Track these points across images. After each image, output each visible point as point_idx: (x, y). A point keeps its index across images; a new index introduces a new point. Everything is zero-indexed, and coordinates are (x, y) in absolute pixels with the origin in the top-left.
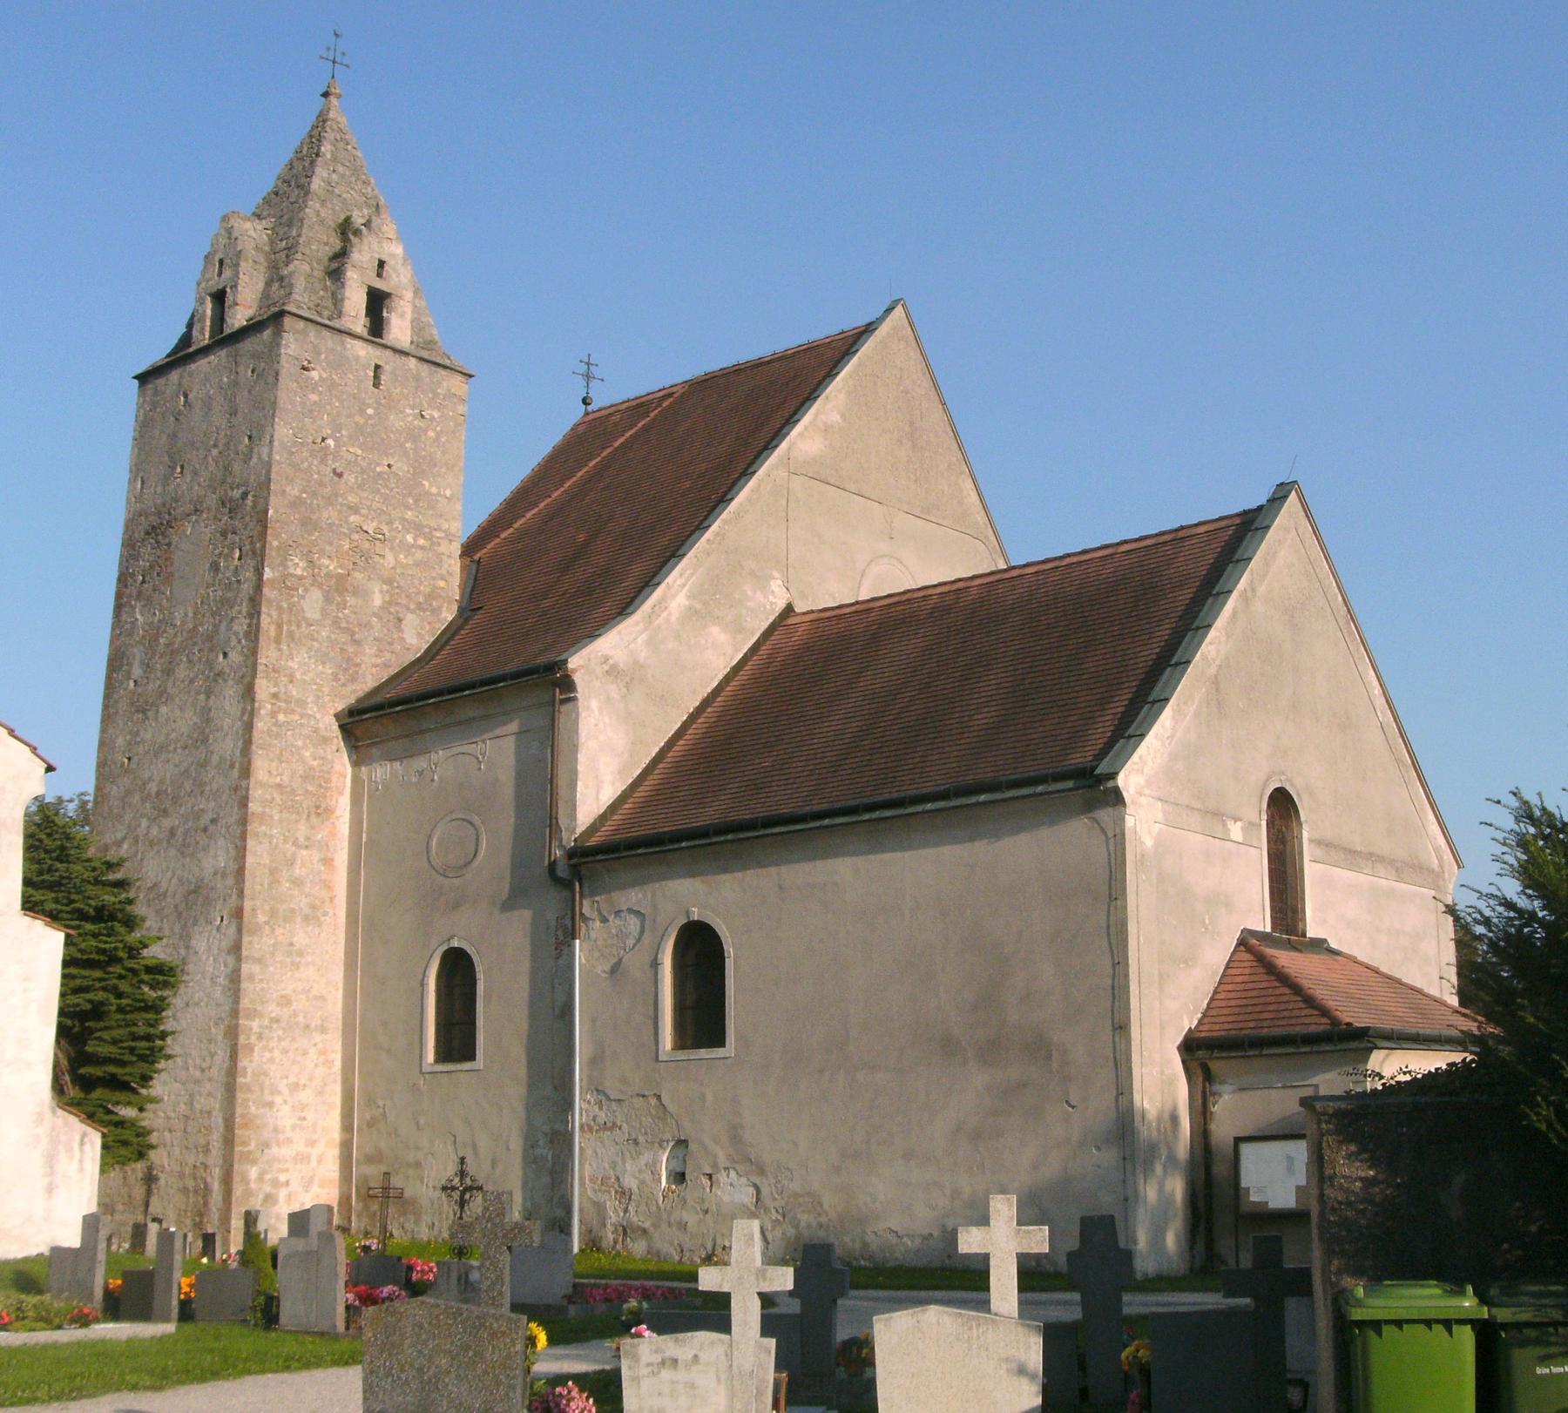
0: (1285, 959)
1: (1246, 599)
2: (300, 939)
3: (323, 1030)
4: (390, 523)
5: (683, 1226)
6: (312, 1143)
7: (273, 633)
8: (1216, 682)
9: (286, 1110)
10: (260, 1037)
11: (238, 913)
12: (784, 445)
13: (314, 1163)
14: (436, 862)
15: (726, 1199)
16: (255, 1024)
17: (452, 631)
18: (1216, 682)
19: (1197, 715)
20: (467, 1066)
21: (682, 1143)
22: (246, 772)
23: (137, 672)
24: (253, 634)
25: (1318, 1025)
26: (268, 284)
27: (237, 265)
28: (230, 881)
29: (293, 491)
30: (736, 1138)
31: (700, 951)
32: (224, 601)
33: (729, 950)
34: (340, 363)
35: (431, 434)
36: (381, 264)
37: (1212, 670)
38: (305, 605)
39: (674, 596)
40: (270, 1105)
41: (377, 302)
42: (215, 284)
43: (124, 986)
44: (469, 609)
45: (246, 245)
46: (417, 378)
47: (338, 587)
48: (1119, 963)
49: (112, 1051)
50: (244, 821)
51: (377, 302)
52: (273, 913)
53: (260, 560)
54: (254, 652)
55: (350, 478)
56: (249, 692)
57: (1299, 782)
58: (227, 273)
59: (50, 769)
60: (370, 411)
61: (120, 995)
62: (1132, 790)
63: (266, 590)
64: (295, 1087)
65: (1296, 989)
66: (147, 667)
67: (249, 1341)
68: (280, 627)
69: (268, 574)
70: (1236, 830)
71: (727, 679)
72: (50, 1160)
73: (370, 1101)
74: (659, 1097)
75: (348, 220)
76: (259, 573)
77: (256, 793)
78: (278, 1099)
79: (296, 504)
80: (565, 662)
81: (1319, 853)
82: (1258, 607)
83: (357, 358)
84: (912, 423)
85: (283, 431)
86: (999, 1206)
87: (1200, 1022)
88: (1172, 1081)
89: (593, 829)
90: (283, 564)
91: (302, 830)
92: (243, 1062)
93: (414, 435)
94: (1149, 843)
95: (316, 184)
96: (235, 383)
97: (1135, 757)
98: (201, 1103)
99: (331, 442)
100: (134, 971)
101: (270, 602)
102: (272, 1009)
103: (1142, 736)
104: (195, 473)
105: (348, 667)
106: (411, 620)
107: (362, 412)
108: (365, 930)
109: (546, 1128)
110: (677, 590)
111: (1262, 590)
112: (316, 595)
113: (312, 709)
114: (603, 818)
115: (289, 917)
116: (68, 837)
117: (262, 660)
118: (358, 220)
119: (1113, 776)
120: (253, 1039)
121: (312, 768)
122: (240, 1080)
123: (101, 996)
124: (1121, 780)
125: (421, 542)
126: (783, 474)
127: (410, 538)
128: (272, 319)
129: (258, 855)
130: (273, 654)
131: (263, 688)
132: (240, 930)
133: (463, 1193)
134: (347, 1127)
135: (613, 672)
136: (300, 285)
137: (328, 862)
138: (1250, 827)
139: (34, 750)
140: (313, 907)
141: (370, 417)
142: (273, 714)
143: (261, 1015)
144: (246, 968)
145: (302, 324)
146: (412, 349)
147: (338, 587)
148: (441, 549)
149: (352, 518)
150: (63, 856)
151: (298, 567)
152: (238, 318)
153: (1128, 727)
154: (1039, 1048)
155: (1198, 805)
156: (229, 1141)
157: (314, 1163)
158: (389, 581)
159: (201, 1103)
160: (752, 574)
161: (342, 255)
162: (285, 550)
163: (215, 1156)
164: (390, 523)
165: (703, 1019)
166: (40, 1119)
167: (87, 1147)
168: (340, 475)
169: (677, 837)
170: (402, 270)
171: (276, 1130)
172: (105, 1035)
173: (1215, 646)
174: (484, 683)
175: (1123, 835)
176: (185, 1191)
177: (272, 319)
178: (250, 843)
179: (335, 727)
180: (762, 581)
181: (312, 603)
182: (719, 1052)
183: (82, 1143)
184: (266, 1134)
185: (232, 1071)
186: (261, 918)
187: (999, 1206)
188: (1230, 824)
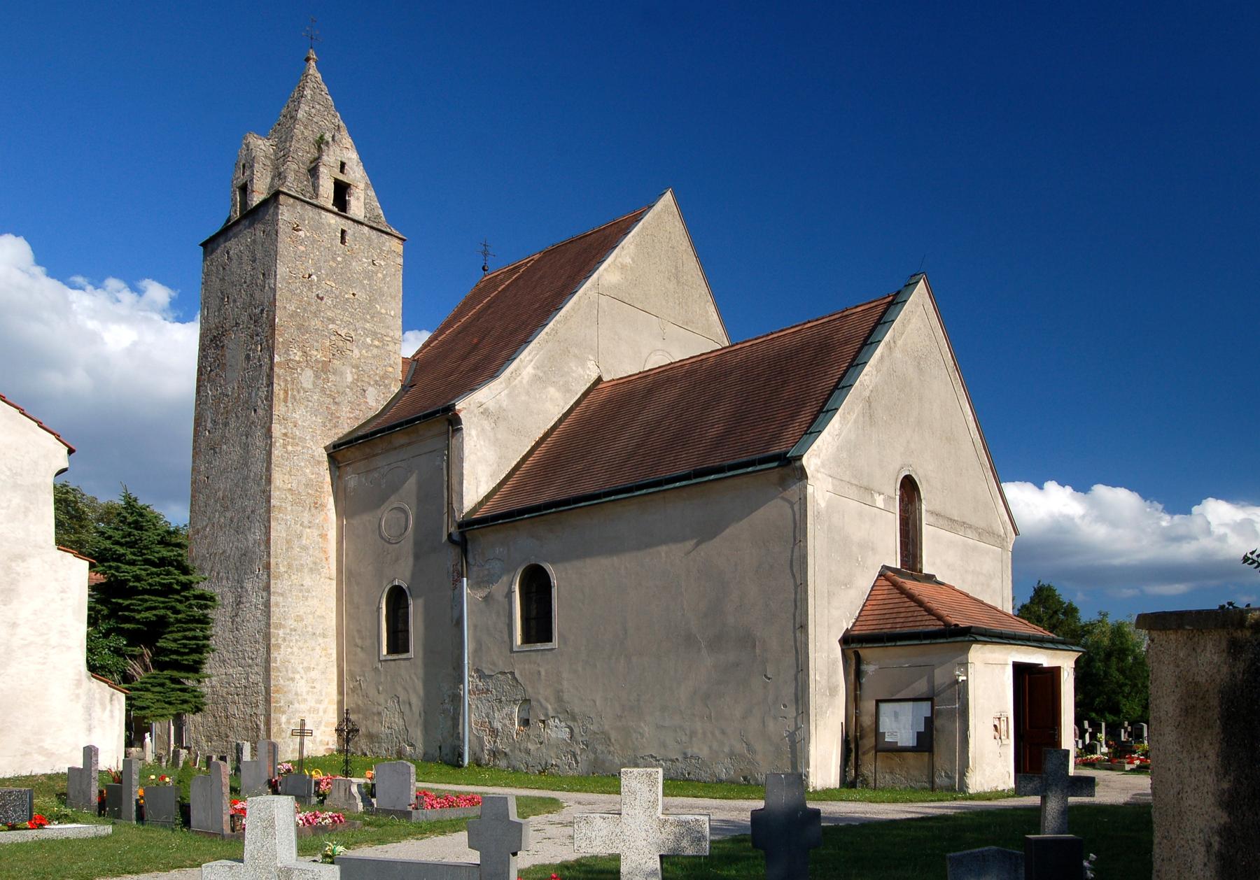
0: (910, 585)
1: (890, 348)
2: (308, 581)
3: (324, 636)
4: (355, 330)
5: (528, 752)
6: (320, 702)
7: (282, 396)
8: (869, 401)
9: (303, 682)
10: (284, 640)
11: (268, 567)
12: (595, 276)
13: (321, 713)
14: (385, 534)
15: (553, 735)
16: (281, 632)
17: (397, 397)
18: (869, 401)
19: (856, 422)
20: (404, 656)
21: (526, 701)
22: (269, 481)
23: (209, 425)
24: (270, 398)
25: (935, 625)
26: (273, 179)
27: (252, 166)
28: (262, 548)
29: (291, 307)
30: (559, 699)
31: (537, 588)
32: (253, 379)
33: (554, 582)
34: (318, 227)
35: (380, 275)
36: (343, 165)
37: (867, 393)
38: (302, 378)
39: (525, 367)
40: (293, 679)
41: (342, 191)
42: (240, 182)
43: (179, 607)
44: (405, 388)
45: (259, 154)
46: (369, 239)
47: (323, 369)
48: (800, 586)
49: (173, 646)
50: (269, 511)
51: (342, 191)
52: (290, 566)
53: (271, 351)
54: (271, 407)
55: (328, 301)
56: (269, 434)
57: (920, 472)
58: (247, 173)
59: (71, 451)
60: (339, 259)
61: (177, 612)
62: (812, 468)
63: (276, 369)
64: (308, 669)
65: (920, 603)
66: (214, 422)
67: (176, 838)
68: (286, 392)
69: (277, 359)
70: (880, 500)
71: (560, 421)
72: (89, 710)
73: (352, 676)
74: (512, 673)
75: (322, 137)
76: (272, 359)
77: (275, 494)
78: (297, 676)
79: (293, 315)
80: (454, 405)
81: (932, 519)
82: (898, 354)
83: (329, 225)
84: (676, 268)
85: (282, 270)
86: (634, 784)
87: (854, 625)
88: (835, 662)
89: (474, 510)
90: (287, 352)
91: (306, 517)
92: (274, 654)
93: (369, 276)
94: (823, 504)
95: (301, 114)
96: (254, 241)
97: (814, 446)
98: (253, 678)
99: (314, 277)
100: (187, 599)
101: (279, 377)
102: (291, 623)
103: (820, 432)
104: (235, 301)
105: (333, 418)
106: (371, 392)
107: (334, 259)
108: (347, 578)
109: (450, 693)
110: (527, 363)
111: (900, 343)
112: (309, 373)
113: (309, 444)
114: (480, 504)
115: (300, 569)
116: (141, 515)
117: (275, 412)
118: (328, 137)
119: (800, 458)
120: (280, 641)
121: (311, 480)
122: (273, 665)
123: (162, 612)
124: (805, 461)
125: (376, 343)
126: (594, 294)
127: (369, 340)
128: (274, 197)
129: (278, 532)
130: (284, 409)
131: (277, 430)
132: (269, 576)
133: (348, 733)
134: (341, 692)
135: (486, 413)
136: (291, 177)
137: (323, 536)
138: (889, 498)
139: (58, 437)
140: (315, 563)
141: (339, 263)
142: (284, 446)
143: (284, 627)
144: (273, 599)
145: (292, 200)
146: (366, 221)
147: (323, 369)
148: (390, 348)
149: (331, 326)
150: (138, 526)
151: (297, 355)
152: (256, 199)
153: (812, 430)
154: (747, 640)
155: (854, 482)
156: (268, 701)
157: (321, 713)
158: (357, 367)
159: (253, 678)
160: (575, 356)
161: (317, 160)
162: (287, 345)
163: (261, 710)
164: (355, 330)
165: (539, 626)
166: (79, 683)
167: (115, 702)
168: (322, 299)
169: (522, 512)
170: (356, 168)
171: (296, 694)
172: (168, 636)
173: (869, 377)
174: (408, 422)
175: (806, 498)
176: (246, 729)
177: (274, 197)
178: (273, 524)
179: (325, 455)
180: (582, 362)
181: (307, 378)
182: (548, 646)
183: (111, 700)
184: (291, 696)
185: (268, 661)
186: (282, 569)
187: (634, 784)
188: (876, 496)
